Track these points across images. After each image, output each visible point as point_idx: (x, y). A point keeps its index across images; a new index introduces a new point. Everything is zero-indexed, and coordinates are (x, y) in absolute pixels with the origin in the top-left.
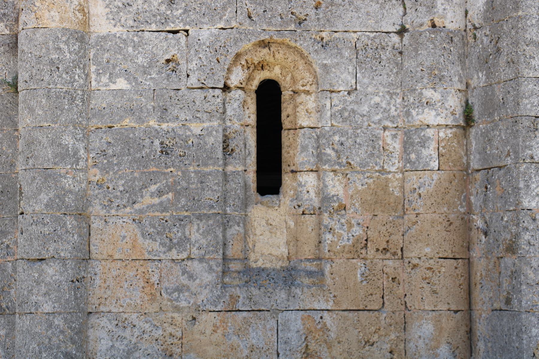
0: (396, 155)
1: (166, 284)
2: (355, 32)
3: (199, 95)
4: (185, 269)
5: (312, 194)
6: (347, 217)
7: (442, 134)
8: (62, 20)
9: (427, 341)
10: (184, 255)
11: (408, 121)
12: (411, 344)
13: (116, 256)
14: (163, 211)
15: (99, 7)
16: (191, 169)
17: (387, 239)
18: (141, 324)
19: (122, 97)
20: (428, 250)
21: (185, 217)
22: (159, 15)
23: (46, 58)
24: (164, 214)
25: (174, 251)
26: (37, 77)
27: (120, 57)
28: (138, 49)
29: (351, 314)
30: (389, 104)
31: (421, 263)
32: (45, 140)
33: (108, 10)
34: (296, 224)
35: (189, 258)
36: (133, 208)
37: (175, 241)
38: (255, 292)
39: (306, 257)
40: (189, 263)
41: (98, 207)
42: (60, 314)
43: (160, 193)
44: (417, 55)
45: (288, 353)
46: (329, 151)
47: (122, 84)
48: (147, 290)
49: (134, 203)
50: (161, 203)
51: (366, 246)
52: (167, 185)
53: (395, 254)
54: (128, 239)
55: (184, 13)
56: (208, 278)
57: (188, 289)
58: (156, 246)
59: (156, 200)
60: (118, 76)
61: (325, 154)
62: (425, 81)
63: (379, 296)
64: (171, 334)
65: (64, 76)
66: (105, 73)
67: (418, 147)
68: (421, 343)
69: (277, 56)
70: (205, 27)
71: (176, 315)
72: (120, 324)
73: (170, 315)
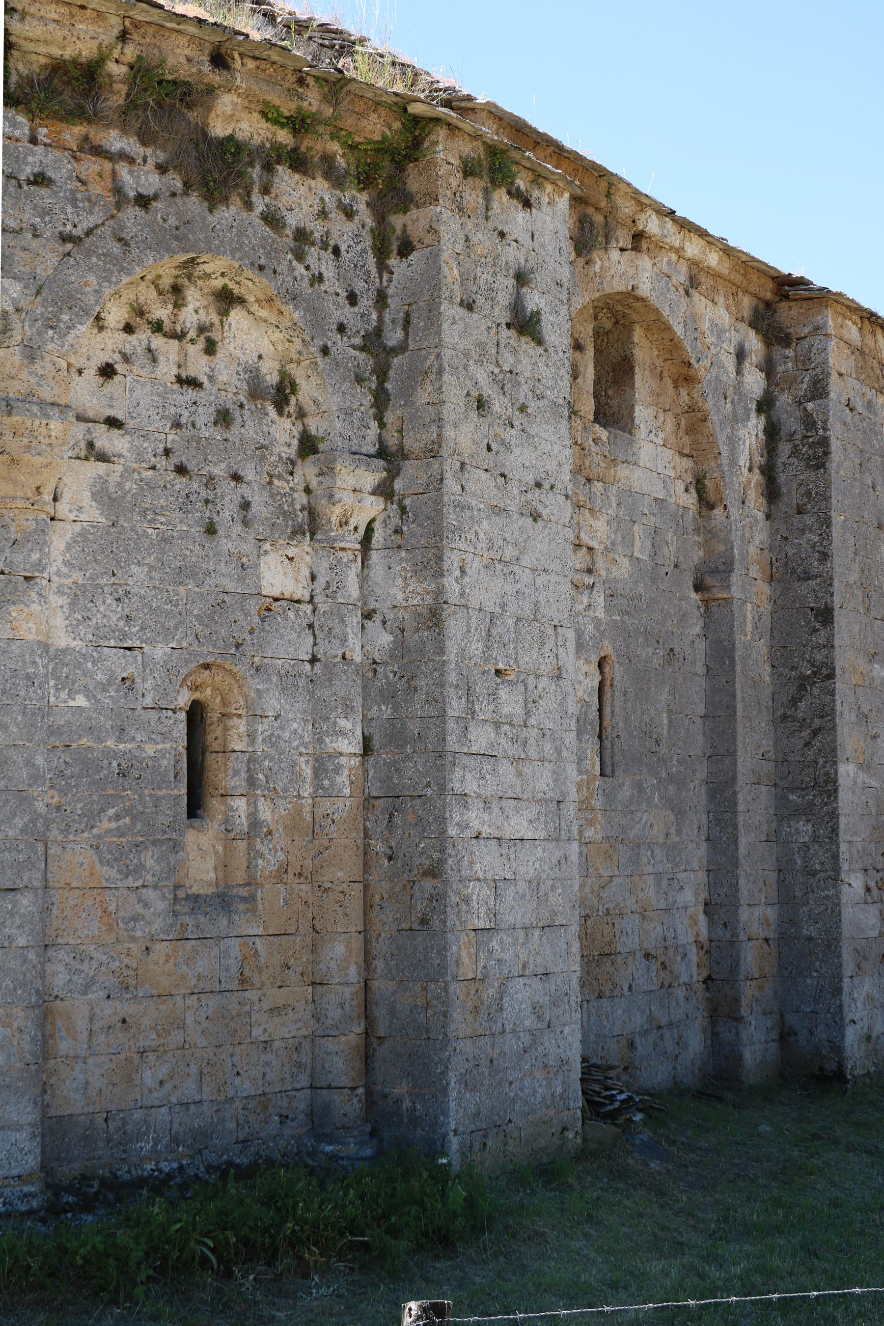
0: (308, 780)
1: (122, 913)
2: (279, 659)
3: (153, 715)
4: (140, 897)
5: (244, 819)
6: (274, 842)
7: (352, 762)
8: (38, 632)
9: (339, 962)
10: (139, 883)
11: (321, 748)
12: (322, 966)
13: (74, 885)
14: (120, 836)
15: (58, 619)
16: (146, 792)
17: (301, 863)
18: (99, 956)
19: (81, 715)
20: (340, 874)
21: (142, 842)
22: (118, 630)
23: (23, 672)
24: (121, 839)
25: (130, 878)
26: (12, 692)
27: (79, 672)
28: (97, 665)
29: (276, 939)
30: (303, 730)
31: (334, 887)
32: (20, 761)
33: (67, 622)
34: (225, 847)
35: (144, 886)
36: (91, 832)
37: (131, 868)
38: (202, 919)
39: (238, 882)
40: (144, 891)
41: (56, 832)
42: (33, 947)
43: (118, 817)
44: (331, 685)
45: (228, 980)
46: (261, 776)
47: (81, 701)
48: (104, 920)
49: (92, 828)
50: (118, 828)
51: (286, 872)
52: (125, 809)
53: (306, 878)
54: (85, 866)
55: (140, 630)
56: (161, 906)
57: (143, 918)
58: (113, 873)
59: (113, 825)
60: (78, 692)
61: (258, 779)
62: (340, 710)
63: (295, 920)
64: (126, 966)
65: (39, 691)
66: (63, 689)
67: (332, 774)
68: (333, 965)
69: (216, 679)
70: (160, 645)
71: (132, 945)
72: (77, 957)
73: (127, 945)
